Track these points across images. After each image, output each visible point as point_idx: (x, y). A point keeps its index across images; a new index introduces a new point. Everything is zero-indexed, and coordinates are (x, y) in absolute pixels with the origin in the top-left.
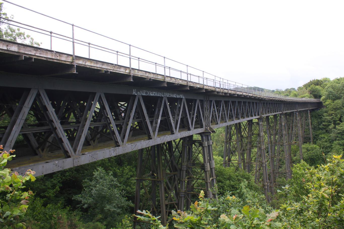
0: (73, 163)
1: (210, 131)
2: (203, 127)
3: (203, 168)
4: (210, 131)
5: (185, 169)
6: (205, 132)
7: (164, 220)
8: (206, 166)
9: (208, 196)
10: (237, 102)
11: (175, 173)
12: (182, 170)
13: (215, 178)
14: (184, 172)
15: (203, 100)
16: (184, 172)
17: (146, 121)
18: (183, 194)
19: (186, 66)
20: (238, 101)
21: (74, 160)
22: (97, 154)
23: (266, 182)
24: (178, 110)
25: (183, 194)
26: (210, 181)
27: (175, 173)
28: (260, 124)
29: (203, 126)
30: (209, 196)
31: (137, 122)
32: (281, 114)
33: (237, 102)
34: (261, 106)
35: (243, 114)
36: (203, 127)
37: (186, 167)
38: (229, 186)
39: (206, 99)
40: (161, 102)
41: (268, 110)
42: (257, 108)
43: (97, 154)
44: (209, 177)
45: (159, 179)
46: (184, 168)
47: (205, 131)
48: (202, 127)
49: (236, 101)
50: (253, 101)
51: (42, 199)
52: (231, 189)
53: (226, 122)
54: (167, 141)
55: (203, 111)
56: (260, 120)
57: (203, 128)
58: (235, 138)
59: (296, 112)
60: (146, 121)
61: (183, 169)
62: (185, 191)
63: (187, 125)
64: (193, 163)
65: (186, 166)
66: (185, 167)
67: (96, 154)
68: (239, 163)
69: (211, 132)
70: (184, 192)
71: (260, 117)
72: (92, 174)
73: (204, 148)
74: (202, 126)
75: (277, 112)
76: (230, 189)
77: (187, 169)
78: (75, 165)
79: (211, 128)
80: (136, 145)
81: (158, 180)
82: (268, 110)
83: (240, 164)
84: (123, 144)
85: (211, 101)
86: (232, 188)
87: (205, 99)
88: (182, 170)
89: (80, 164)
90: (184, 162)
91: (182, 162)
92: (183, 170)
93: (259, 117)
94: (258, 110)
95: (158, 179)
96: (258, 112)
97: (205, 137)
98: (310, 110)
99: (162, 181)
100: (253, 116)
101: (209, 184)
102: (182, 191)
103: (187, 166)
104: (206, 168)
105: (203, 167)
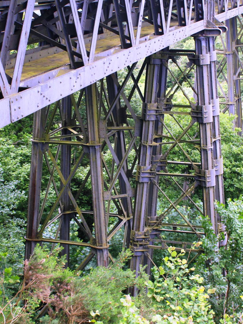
0: (9, 113)
1: (219, 29)
3: (197, 117)
4: (219, 29)
5: (153, 118)
6: (207, 30)
7: (101, 236)
8: (205, 111)
9: (208, 180)
11: (118, 128)
12: (146, 121)
13: (211, 149)
14: (151, 124)
16: (151, 124)
17: (68, 5)
18: (147, 175)
21: (12, 105)
22: (50, 87)
25: (147, 175)
27: (118, 128)
29: (202, 14)
30: (208, 182)
31: (42, 8)
36: (202, 19)
37: (155, 114)
38: (228, 155)
43: (50, 87)
44: (211, 138)
45: (90, 142)
46: (151, 117)
47: (207, 26)
51: (214, 305)
52: (234, 163)
57: (203, 20)
58: (224, 46)
60: (68, 5)
61: (147, 118)
62: (151, 170)
64: (166, 105)
65: (156, 112)
67: (49, 87)
68: (230, 103)
70: (149, 171)
73: (202, 68)
76: (231, 162)
77: (157, 117)
78: (13, 118)
79: (216, 22)
80: (111, 62)
81: (88, 144)
83: (231, 105)
84: (88, 60)
86: (235, 161)
88: (146, 121)
89: (22, 114)
90: (151, 102)
95: (87, 141)
97: (206, 42)
99: (96, 147)
101: (211, 153)
102: (143, 170)
103: (156, 111)
104: (205, 116)
105: (197, 113)
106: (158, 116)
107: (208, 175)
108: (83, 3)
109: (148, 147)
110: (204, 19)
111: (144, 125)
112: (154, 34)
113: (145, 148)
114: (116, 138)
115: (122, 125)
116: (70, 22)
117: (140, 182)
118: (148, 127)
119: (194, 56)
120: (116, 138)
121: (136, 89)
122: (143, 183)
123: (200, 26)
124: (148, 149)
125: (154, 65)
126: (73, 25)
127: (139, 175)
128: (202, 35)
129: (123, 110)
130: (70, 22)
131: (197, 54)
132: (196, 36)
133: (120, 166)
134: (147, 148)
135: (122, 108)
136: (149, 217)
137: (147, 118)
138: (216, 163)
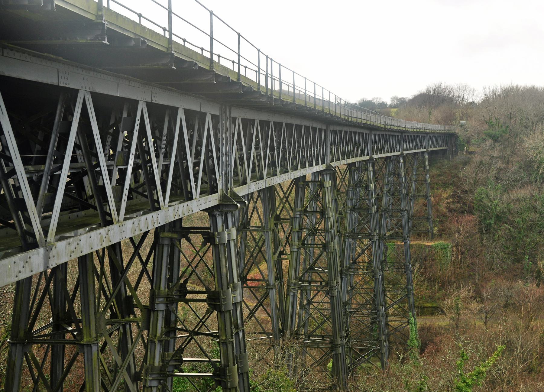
2: (217, 192)
10: (257, 124)
15: (219, 116)
19: (209, 13)
20: (260, 121)
23: (381, 305)
24: (165, 142)
26: (232, 338)
28: (325, 186)
32: (368, 160)
33: (257, 124)
34: (329, 137)
35: (273, 164)
36: (217, 192)
39: (225, 113)
40: (69, 113)
41: (273, 156)
42: (341, 138)
47: (223, 200)
48: (213, 190)
49: (254, 121)
50: (290, 121)
53: (263, 178)
54: (157, 225)
55: (218, 149)
56: (369, 162)
59: (323, 176)
61: (156, 308)
63: (97, 205)
66: (295, 247)
69: (239, 205)
71: (401, 153)
72: (240, 231)
73: (218, 247)
74: (216, 190)
75: (394, 152)
77: (167, 306)
79: (235, 195)
82: (273, 156)
85: (234, 120)
87: (223, 115)
91: (154, 288)
92: (158, 311)
93: (324, 168)
94: (323, 148)
96: (323, 155)
97: (222, 219)
98: (428, 154)
100: (307, 166)
106: (169, 305)
107: (229, 373)
108: (43, 174)
109: (157, 342)
110: (219, 192)
111: (152, 316)
112: (21, 247)
113: (153, 344)
114: (121, 332)
115: (129, 317)
116: (100, 184)
117: (147, 386)
118: (157, 318)
119: (208, 233)
120: (121, 332)
121: (144, 274)
122: (151, 387)
123: (213, 200)
124: (157, 344)
125: (163, 245)
126: (103, 187)
127: (145, 378)
128: (217, 210)
129: (129, 299)
130: (100, 184)
131: (212, 231)
132: (210, 211)
133: (122, 368)
134: (155, 343)
135: (129, 296)
136: (466, 251)
137: (156, 307)
138: (240, 359)
